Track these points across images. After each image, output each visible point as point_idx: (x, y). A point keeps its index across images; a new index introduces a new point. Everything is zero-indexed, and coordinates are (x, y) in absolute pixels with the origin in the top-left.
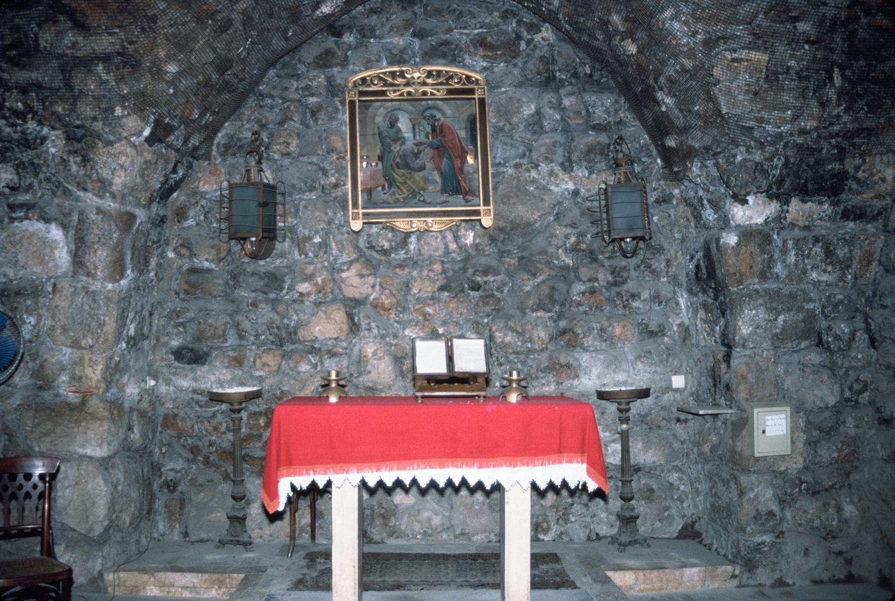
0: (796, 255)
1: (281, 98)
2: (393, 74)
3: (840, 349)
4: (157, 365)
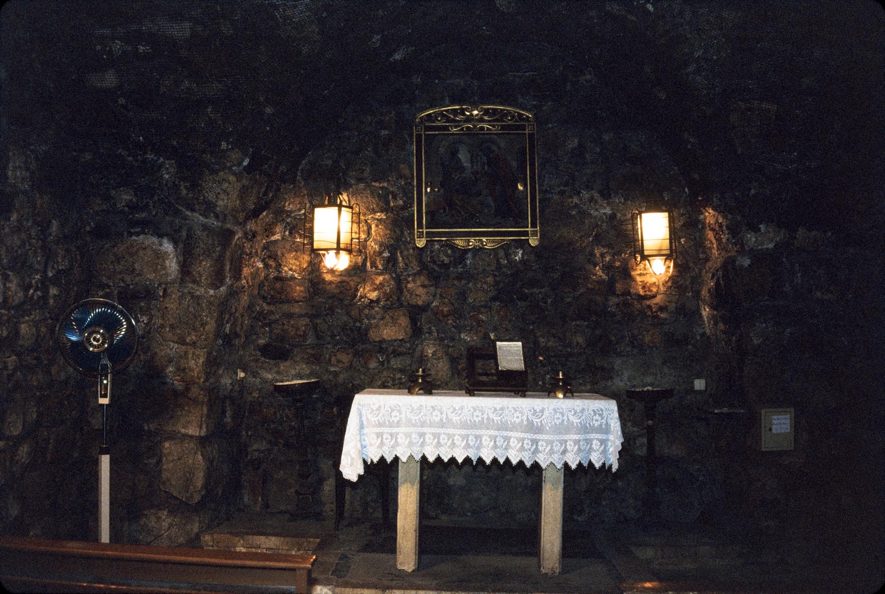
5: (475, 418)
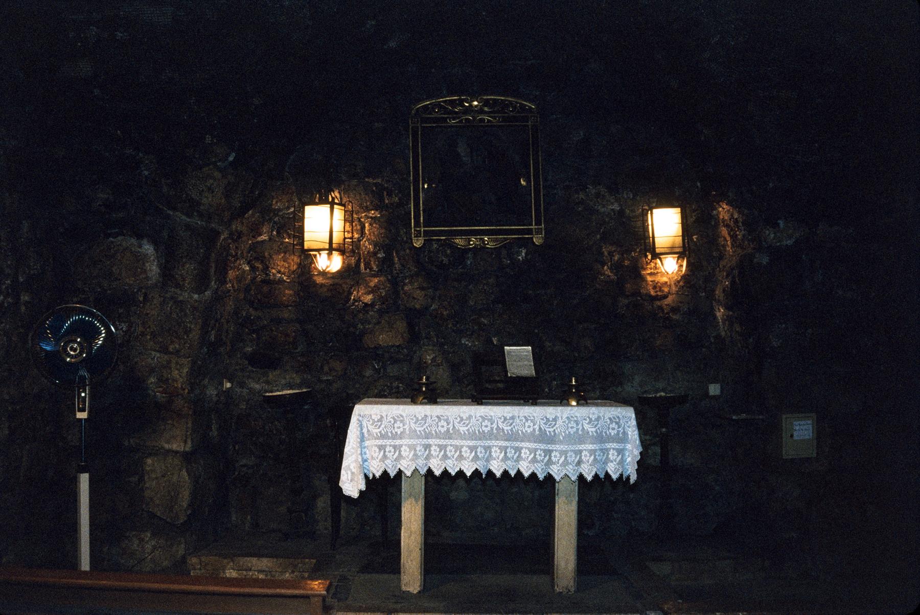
2: (452, 103)
5: (484, 428)
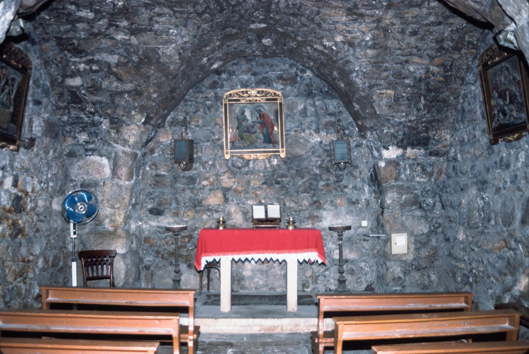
0: (410, 171)
1: (195, 102)
2: (243, 92)
3: (429, 210)
4: (142, 216)
